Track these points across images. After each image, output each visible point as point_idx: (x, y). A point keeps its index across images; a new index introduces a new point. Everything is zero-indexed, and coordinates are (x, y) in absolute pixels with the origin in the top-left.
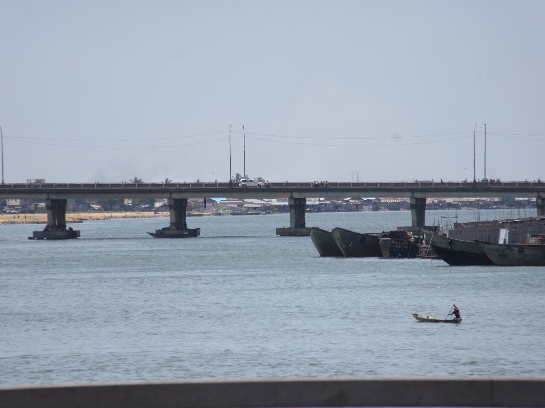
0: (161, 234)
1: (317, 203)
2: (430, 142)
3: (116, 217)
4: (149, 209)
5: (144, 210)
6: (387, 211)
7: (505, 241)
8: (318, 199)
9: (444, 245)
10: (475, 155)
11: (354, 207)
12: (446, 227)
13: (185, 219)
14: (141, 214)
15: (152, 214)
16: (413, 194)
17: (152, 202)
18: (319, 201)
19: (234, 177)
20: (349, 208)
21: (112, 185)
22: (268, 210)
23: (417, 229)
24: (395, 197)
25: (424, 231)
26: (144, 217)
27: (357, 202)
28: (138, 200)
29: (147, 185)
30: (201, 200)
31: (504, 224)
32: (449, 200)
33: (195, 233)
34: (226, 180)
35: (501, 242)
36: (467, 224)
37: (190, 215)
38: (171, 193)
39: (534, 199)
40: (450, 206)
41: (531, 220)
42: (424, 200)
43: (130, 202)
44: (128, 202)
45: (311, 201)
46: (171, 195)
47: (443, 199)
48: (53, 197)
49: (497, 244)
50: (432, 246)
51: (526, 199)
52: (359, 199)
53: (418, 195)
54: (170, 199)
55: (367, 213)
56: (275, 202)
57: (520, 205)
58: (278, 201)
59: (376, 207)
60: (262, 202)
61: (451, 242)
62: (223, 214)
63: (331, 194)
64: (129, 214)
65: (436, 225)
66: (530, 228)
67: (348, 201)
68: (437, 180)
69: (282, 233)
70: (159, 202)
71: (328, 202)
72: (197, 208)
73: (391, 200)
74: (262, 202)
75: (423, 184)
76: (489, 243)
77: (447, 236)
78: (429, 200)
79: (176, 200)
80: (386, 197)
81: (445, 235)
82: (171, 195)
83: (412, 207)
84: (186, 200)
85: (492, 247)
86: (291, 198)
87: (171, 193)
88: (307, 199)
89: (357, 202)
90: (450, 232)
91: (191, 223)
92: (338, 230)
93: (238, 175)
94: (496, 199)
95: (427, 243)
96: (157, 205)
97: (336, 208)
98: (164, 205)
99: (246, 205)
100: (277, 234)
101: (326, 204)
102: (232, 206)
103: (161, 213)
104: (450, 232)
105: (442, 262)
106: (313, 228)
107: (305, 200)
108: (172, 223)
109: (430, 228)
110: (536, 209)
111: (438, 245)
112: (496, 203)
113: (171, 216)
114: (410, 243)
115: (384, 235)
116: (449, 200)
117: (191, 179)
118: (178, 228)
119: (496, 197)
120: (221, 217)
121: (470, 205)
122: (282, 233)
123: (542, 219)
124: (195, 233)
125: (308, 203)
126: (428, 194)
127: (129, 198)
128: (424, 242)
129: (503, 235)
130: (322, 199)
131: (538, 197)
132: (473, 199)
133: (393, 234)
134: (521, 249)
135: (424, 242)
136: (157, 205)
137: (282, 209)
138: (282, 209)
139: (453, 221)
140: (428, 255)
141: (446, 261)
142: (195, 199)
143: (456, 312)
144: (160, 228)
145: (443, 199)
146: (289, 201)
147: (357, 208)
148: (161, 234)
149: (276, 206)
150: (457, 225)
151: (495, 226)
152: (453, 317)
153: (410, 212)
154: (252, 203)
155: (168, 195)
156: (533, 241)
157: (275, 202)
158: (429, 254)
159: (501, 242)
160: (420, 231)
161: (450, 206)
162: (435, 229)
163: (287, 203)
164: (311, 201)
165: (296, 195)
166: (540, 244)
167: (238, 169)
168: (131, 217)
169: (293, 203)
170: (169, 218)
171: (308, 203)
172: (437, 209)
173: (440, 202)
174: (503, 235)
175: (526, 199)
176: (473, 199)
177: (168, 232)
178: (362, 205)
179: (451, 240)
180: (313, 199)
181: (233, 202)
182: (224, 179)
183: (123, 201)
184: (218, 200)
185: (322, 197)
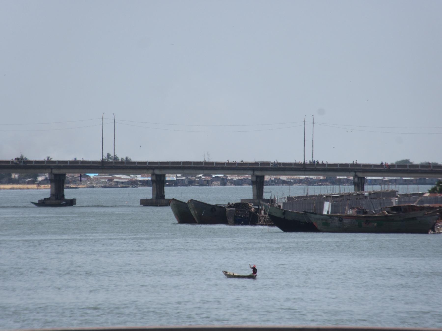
0: (43, 203)
1: (175, 179)
2: (187, 125)
3: (4, 189)
4: (32, 182)
5: (29, 183)
6: (233, 186)
7: (328, 212)
8: (175, 175)
9: (278, 214)
10: (102, 138)
11: (205, 182)
12: (281, 200)
13: (63, 191)
14: (26, 186)
15: (35, 186)
16: (153, 171)
17: (36, 176)
18: (177, 177)
19: (105, 156)
20: (202, 183)
21: (37, 162)
22: (134, 184)
23: (257, 201)
24: (239, 175)
25: (262, 203)
26: (28, 189)
27: (208, 178)
28: (24, 175)
29: (134, 163)
30: (77, 175)
31: (328, 198)
32: (284, 178)
33: (71, 203)
34: (99, 159)
35: (325, 213)
36: (297, 198)
37: (68, 188)
38: (52, 169)
39: (352, 178)
40: (284, 182)
41: (349, 195)
42: (263, 177)
43: (17, 176)
44: (15, 176)
45: (169, 177)
46: (254, 173)
47: (278, 177)
48: (56, 171)
49: (321, 214)
50: (270, 215)
51: (345, 177)
52: (209, 175)
53: (258, 173)
54: (51, 174)
55: (216, 188)
56: (139, 178)
57: (340, 182)
58: (142, 177)
59: (224, 182)
60: (129, 177)
61: (284, 213)
62: (95, 187)
63: (186, 171)
64: (15, 186)
65: (273, 198)
66: (349, 202)
67: (200, 177)
68: (239, 160)
69: (145, 203)
70: (41, 176)
71: (184, 178)
72: (74, 182)
73: (235, 178)
74: (129, 177)
75: (263, 164)
76: (315, 214)
77: (282, 207)
78: (267, 178)
79: (56, 175)
80: (232, 174)
81: (280, 206)
82: (254, 173)
83: (253, 183)
84: (65, 175)
85: (317, 216)
86: (153, 174)
87: (52, 169)
88: (167, 175)
89: (208, 178)
90: (284, 204)
91: (68, 194)
92: (192, 201)
93: (108, 155)
94: (322, 178)
95: (265, 213)
96: (40, 179)
97: (191, 183)
98: (46, 179)
99: (115, 180)
100: (141, 204)
101: (182, 180)
102: (103, 180)
103: (42, 186)
104: (284, 204)
105: (276, 229)
106: (173, 199)
107: (164, 176)
108: (52, 195)
109: (268, 201)
110: (353, 186)
111: (274, 214)
112: (321, 181)
113: (51, 188)
114: (251, 212)
115: (230, 206)
116: (284, 178)
117: (69, 158)
118: (57, 199)
119: (321, 175)
120: (94, 189)
121: (300, 182)
122: (145, 203)
123: (358, 195)
124: (71, 203)
125: (167, 179)
126: (266, 172)
127: (16, 173)
128: (262, 212)
129: (327, 207)
130: (179, 175)
131: (355, 176)
132: (303, 177)
133: (237, 205)
134: (341, 219)
135: (262, 212)
136: (40, 179)
137: (144, 183)
138: (144, 183)
139: (286, 195)
140: (265, 223)
141: (283, 231)
142: (72, 175)
143: (255, 270)
144: (42, 198)
145: (278, 177)
146: (151, 177)
147: (208, 183)
148: (43, 203)
149: (140, 181)
150: (289, 198)
151: (321, 200)
152: (251, 272)
153: (251, 187)
154: (120, 178)
155: (50, 170)
156: (350, 212)
157: (139, 178)
158: (266, 222)
159: (325, 213)
160: (259, 203)
161: (284, 182)
162: (272, 201)
163: (150, 179)
164: (169, 177)
165: (157, 172)
166: (356, 215)
167: (109, 150)
168: (17, 189)
169: (154, 178)
170: (49, 190)
171: (167, 179)
172: (273, 185)
173: (275, 179)
174: (327, 207)
175: (345, 177)
176: (303, 177)
177: (48, 202)
178: (212, 181)
179: (285, 211)
180: (171, 176)
181: (104, 177)
182: (97, 158)
183: (10, 175)
184: (92, 175)
185: (179, 173)
